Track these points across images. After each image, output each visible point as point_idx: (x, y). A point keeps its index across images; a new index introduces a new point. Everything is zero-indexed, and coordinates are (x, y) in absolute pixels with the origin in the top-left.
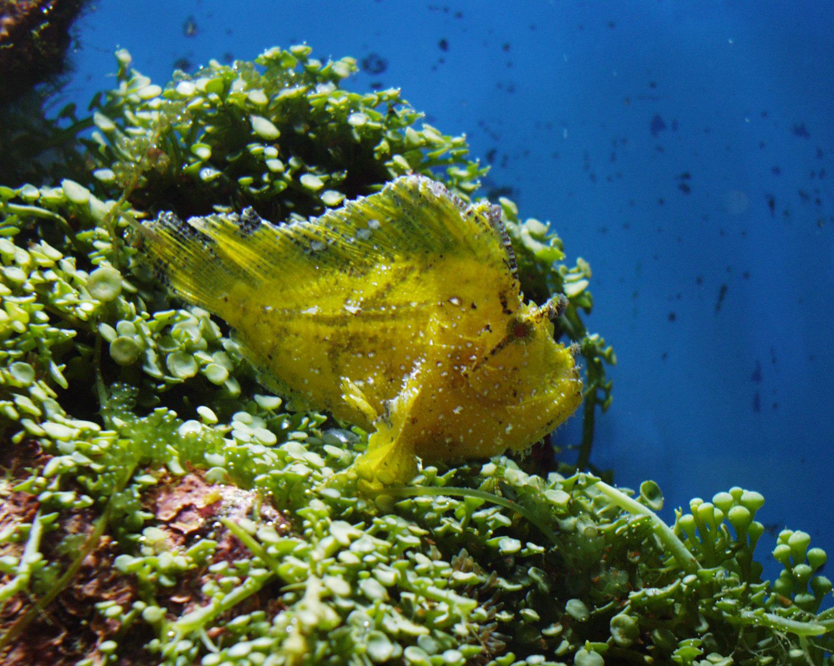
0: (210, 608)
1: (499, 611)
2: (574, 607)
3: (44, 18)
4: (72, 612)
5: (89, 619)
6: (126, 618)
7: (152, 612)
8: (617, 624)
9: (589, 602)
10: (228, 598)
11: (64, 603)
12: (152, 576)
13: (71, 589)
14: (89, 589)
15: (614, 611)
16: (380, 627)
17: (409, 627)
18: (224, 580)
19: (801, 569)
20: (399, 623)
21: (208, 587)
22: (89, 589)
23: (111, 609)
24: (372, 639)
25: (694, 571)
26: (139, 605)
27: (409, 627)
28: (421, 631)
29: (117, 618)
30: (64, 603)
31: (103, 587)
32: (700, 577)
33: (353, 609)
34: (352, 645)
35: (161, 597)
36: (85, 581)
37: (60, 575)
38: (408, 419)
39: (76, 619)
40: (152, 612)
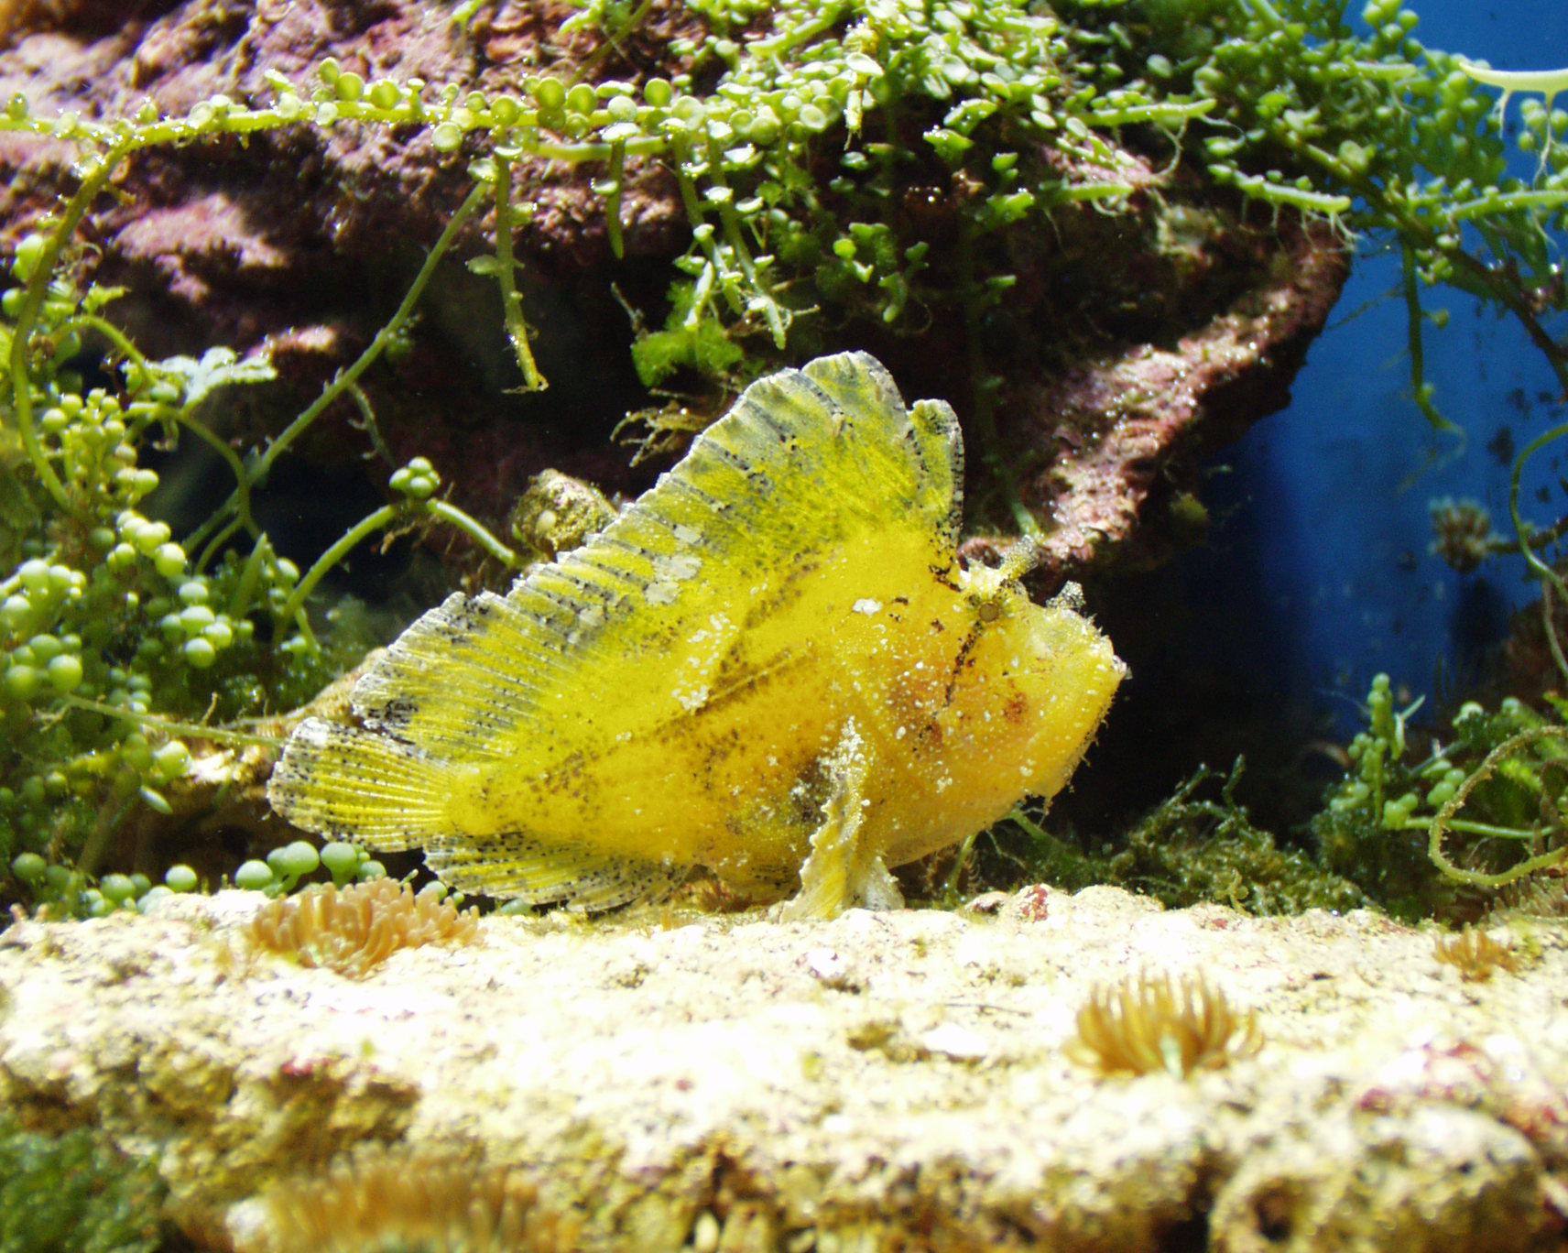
0: (782, 37)
1: (1081, 61)
2: (1158, 64)
3: (435, 166)
4: (647, 53)
5: (664, 59)
6: (700, 54)
7: (725, 46)
8: (1203, 78)
9: (1172, 58)
10: (798, 30)
11: (639, 45)
12: (724, 14)
13: (643, 31)
14: (662, 30)
15: (1197, 66)
16: (956, 52)
17: (985, 57)
18: (796, 12)
19: (1391, 31)
20: (973, 52)
21: (779, 19)
22: (662, 30)
23: (683, 44)
24: (948, 61)
25: (1279, 27)
26: (712, 39)
27: (985, 57)
28: (1000, 62)
29: (690, 53)
30: (639, 45)
31: (676, 28)
32: (1288, 34)
33: (927, 35)
34: (927, 62)
35: (736, 33)
36: (659, 21)
37: (633, 11)
38: (1190, 1165)
39: (651, 61)
40: (725, 46)
